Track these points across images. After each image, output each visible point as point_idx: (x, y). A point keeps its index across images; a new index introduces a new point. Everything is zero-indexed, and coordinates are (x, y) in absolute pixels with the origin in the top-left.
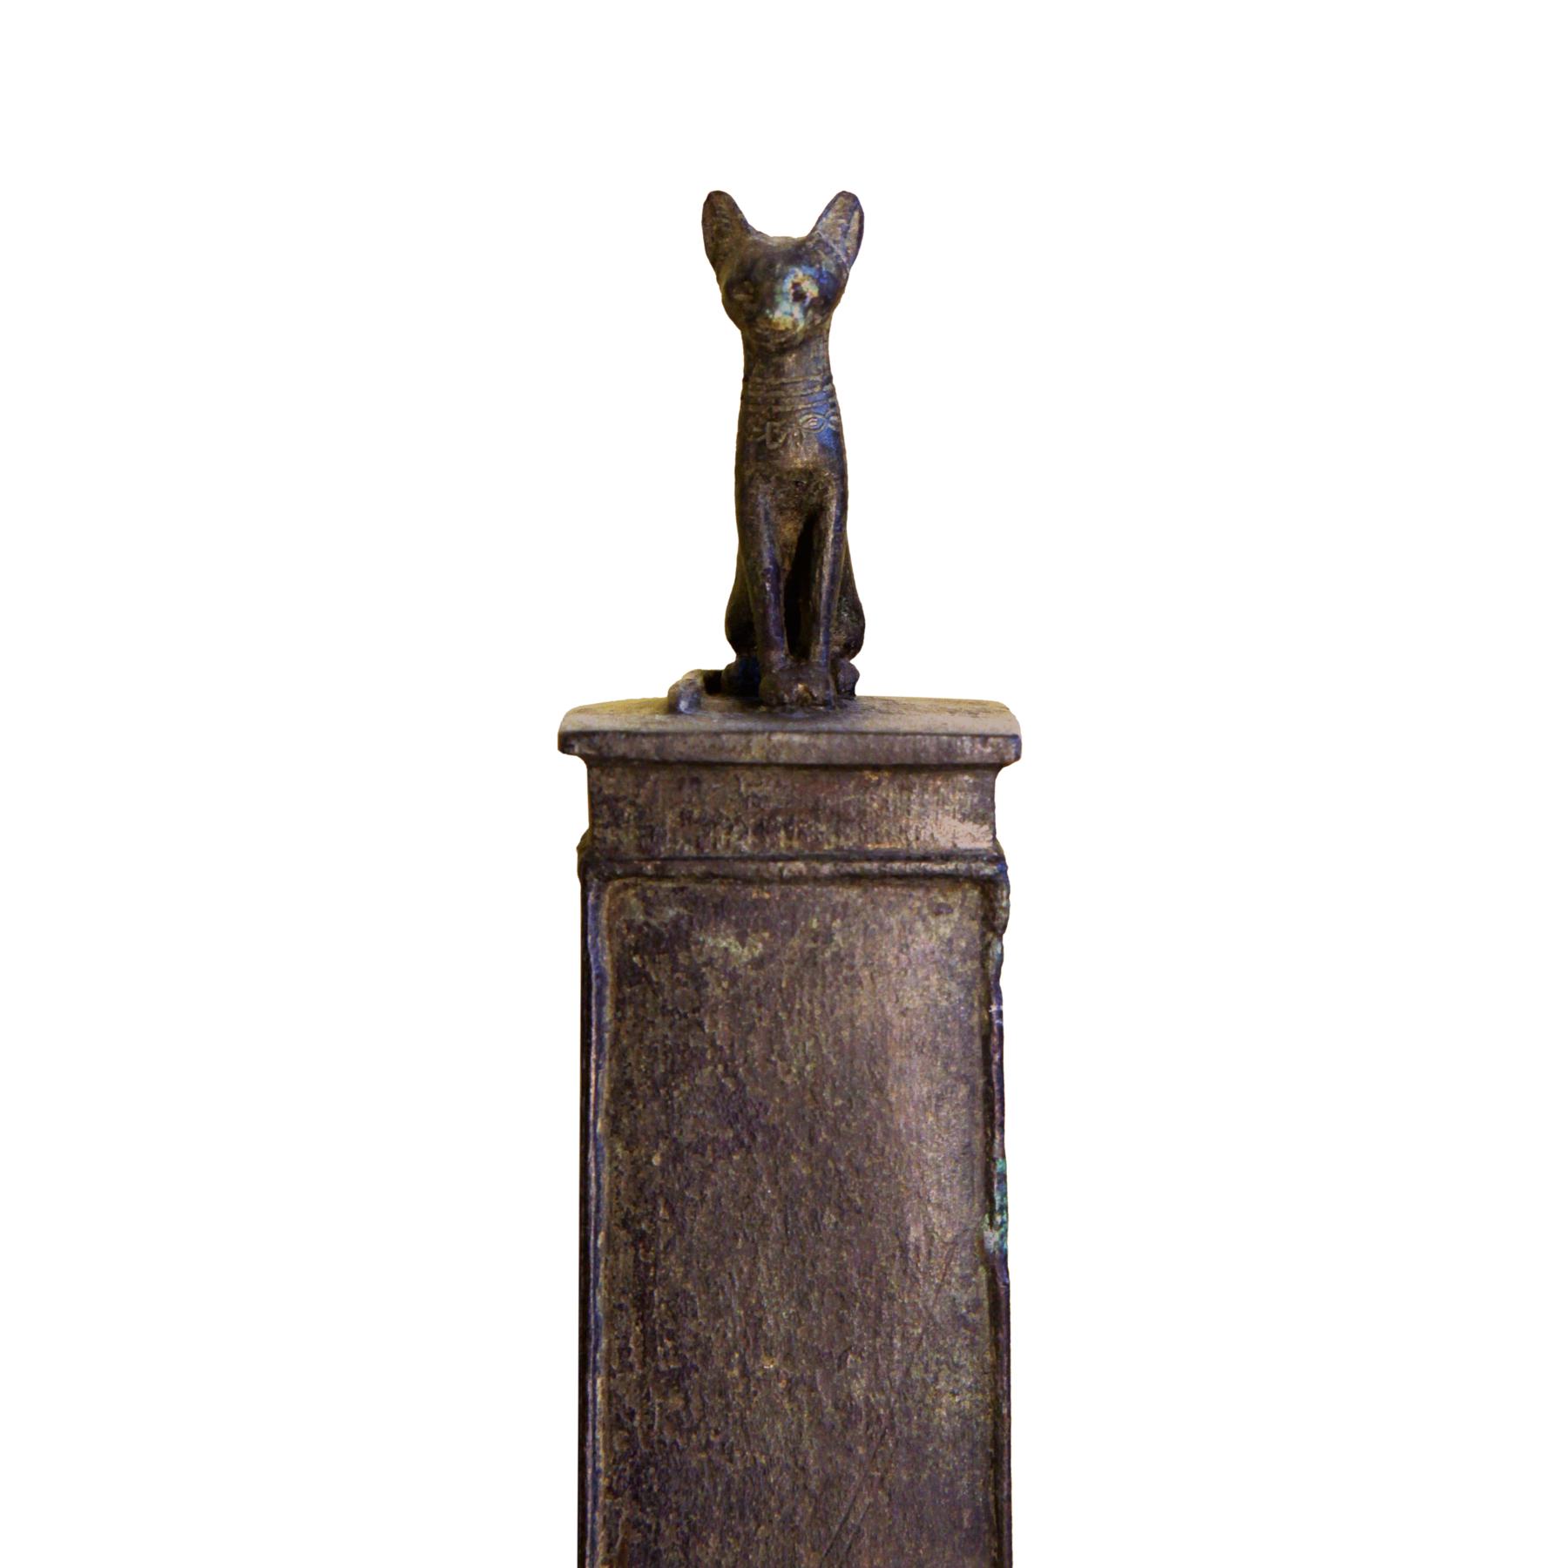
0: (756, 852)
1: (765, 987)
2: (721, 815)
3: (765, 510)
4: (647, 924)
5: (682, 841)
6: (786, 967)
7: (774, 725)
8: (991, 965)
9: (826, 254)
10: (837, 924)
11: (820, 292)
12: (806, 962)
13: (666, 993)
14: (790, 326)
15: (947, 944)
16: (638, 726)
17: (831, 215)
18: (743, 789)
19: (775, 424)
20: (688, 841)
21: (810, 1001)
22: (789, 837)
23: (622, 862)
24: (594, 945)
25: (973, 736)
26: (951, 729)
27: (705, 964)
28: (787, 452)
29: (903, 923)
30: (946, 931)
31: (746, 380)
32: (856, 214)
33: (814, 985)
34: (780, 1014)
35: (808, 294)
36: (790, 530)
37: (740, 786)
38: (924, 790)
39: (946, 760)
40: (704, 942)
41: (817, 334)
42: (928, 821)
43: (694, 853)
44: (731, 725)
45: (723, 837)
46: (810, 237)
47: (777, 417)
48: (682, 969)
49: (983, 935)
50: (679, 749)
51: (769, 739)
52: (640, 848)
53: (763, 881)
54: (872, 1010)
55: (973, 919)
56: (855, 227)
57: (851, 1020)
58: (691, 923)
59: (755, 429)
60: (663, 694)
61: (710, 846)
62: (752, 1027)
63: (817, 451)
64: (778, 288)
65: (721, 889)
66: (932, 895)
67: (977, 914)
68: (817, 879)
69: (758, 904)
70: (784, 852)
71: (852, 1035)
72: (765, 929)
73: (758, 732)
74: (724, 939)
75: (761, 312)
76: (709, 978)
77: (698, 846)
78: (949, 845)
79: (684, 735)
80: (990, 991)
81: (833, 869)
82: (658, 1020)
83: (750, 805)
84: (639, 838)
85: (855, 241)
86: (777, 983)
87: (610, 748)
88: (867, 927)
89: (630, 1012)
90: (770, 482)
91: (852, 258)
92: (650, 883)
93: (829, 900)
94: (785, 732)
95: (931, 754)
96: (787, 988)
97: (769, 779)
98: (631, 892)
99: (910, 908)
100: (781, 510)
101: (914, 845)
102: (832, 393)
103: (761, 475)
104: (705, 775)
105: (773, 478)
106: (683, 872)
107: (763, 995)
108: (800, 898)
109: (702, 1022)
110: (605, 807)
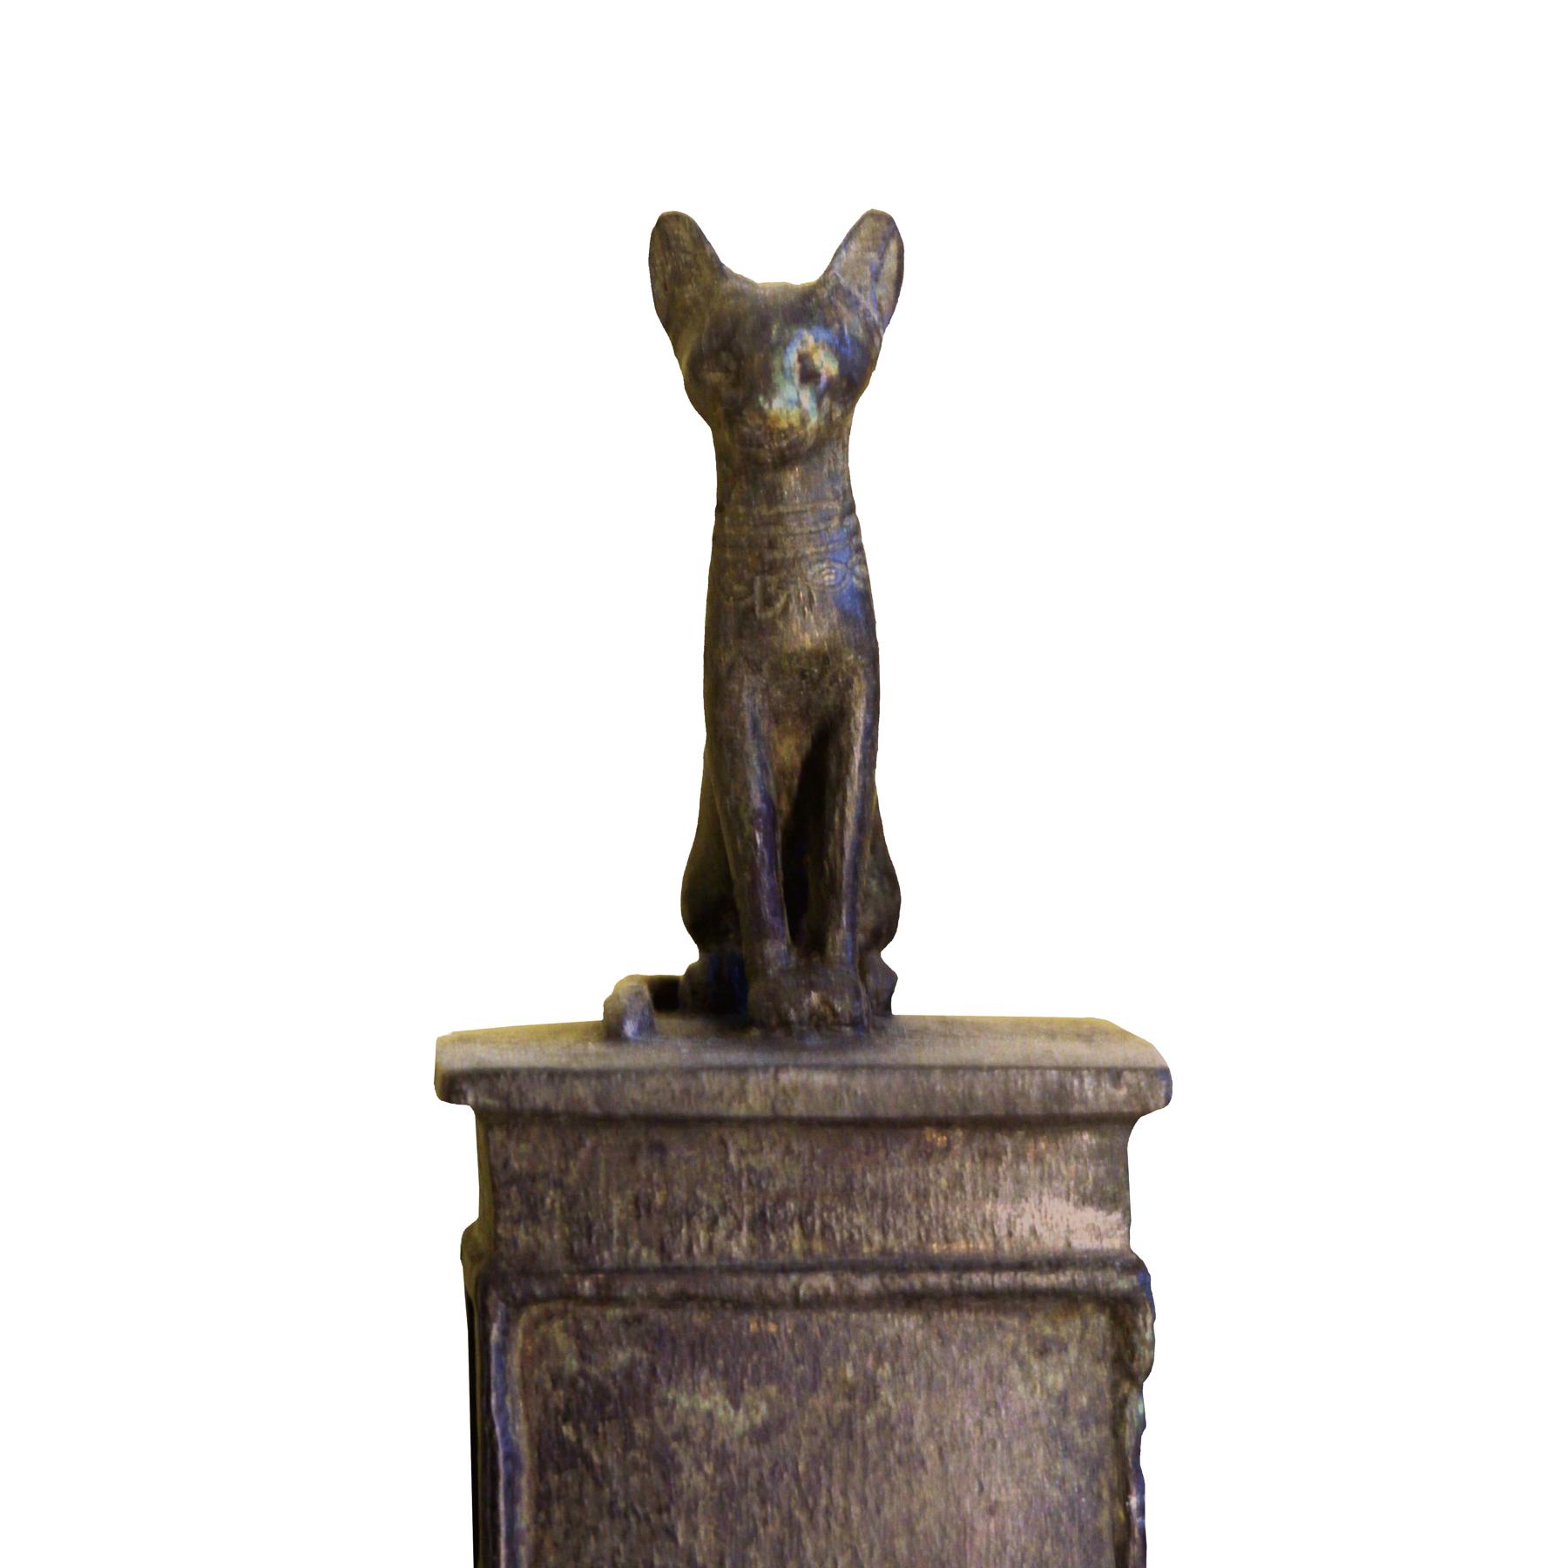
0: (755, 1258)
1: (772, 1473)
2: (698, 1203)
3: (752, 715)
4: (582, 1373)
5: (636, 1243)
6: (804, 1441)
7: (778, 1058)
8: (1128, 1433)
9: (848, 307)
10: (885, 1371)
11: (840, 366)
12: (835, 1433)
13: (615, 1482)
14: (795, 421)
15: (1059, 1401)
16: (564, 1060)
17: (853, 246)
18: (733, 1158)
19: (768, 578)
20: (646, 1242)
21: (844, 1494)
22: (807, 1235)
23: (541, 1276)
24: (501, 1407)
25: (1099, 1072)
26: (1062, 1061)
27: (677, 1437)
28: (788, 623)
29: (988, 1368)
30: (1056, 1380)
31: (720, 510)
32: (893, 247)
33: (849, 1467)
34: (797, 1513)
35: (823, 371)
36: (790, 750)
37: (727, 1154)
38: (1020, 1156)
39: (1056, 1109)
40: (674, 1402)
41: (835, 434)
42: (1027, 1206)
43: (656, 1260)
44: (711, 1057)
45: (702, 1235)
46: (822, 282)
47: (772, 568)
48: (639, 1444)
49: (1115, 1386)
50: (635, 1097)
51: (776, 1079)
52: (571, 1255)
53: (765, 1305)
54: (942, 1506)
55: (1098, 1360)
56: (890, 264)
57: (909, 1524)
58: (653, 1372)
59: (737, 588)
60: (597, 1015)
61: (683, 1250)
62: (752, 1535)
63: (835, 621)
64: (776, 363)
65: (699, 1319)
66: (1034, 1323)
67: (1104, 1352)
68: (852, 1302)
69: (761, 1343)
70: (799, 1257)
71: (910, 1546)
72: (770, 1380)
73: (756, 1068)
74: (705, 1397)
75: (750, 399)
76: (685, 1458)
77: (662, 1250)
78: (1061, 1244)
79: (641, 1074)
80: (1129, 1478)
81: (877, 1282)
82: (604, 1525)
83: (744, 1184)
84: (569, 1240)
85: (890, 288)
86: (790, 1465)
87: (522, 1094)
88: (930, 1378)
89: (558, 1514)
90: (760, 670)
91: (886, 319)
92: (587, 1308)
93: (872, 1332)
94: (798, 1067)
95: (1033, 1104)
96: (807, 1472)
97: (773, 1144)
98: (557, 1325)
99: (1001, 1346)
100: (777, 718)
101: (1006, 1246)
102: (856, 531)
103: (746, 658)
104: (673, 1139)
105: (765, 666)
106: (640, 1290)
107: (769, 1485)
108: (825, 1332)
109: (673, 1526)
110: (514, 1189)
